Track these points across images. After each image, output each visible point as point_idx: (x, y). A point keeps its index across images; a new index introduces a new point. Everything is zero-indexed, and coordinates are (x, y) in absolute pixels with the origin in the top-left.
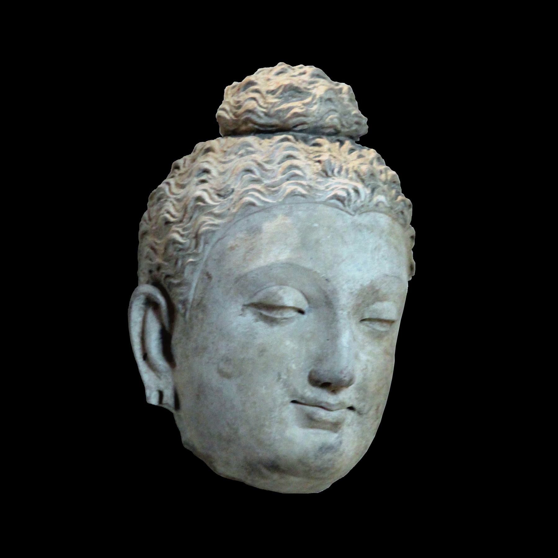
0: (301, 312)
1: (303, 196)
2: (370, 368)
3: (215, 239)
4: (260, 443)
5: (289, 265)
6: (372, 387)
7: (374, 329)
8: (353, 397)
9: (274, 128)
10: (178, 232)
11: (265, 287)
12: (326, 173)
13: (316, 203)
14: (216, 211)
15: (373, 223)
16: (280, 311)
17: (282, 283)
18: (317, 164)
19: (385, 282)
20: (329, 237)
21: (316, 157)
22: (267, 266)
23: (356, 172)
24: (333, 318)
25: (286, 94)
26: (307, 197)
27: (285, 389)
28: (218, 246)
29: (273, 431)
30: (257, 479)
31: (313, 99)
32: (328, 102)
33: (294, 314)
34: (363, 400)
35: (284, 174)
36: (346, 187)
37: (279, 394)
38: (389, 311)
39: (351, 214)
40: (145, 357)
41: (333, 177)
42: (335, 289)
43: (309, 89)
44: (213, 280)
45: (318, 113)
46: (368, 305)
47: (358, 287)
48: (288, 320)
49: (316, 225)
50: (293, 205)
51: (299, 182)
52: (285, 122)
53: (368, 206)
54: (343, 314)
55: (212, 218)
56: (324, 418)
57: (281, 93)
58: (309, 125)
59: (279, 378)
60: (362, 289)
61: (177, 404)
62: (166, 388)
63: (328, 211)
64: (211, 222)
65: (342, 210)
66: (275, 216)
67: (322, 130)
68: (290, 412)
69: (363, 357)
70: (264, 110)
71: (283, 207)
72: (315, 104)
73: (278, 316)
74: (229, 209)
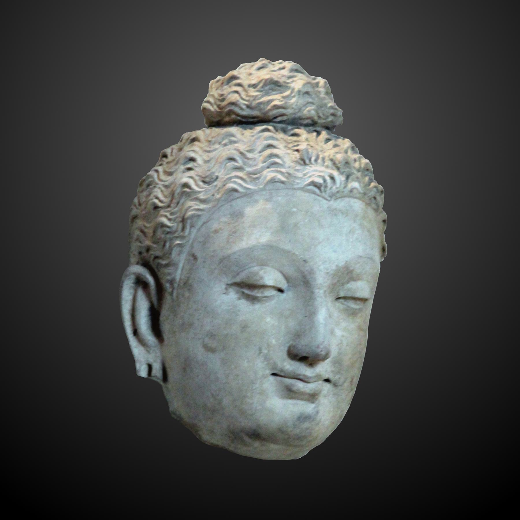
0: (281, 291)
1: (282, 182)
2: (345, 343)
3: (200, 223)
4: (242, 413)
5: (269, 247)
6: (346, 361)
7: (348, 307)
8: (329, 370)
9: (255, 120)
10: (166, 216)
11: (247, 267)
12: (304, 162)
13: (295, 189)
14: (202, 196)
15: (348, 208)
16: (261, 290)
17: (263, 264)
18: (296, 153)
19: (359, 263)
20: (306, 221)
21: (294, 146)
22: (249, 248)
23: (332, 160)
24: (310, 297)
25: (267, 88)
26: (286, 184)
27: (266, 363)
28: (203, 229)
29: (254, 402)
30: (239, 446)
31: (292, 93)
32: (306, 95)
33: (274, 292)
34: (339, 372)
35: (264, 162)
36: (322, 174)
37: (260, 367)
38: (362, 290)
39: (327, 200)
40: (136, 332)
41: (311, 165)
42: (312, 270)
43: (288, 83)
44: (199, 261)
45: (296, 105)
46: (343, 284)
47: (334, 268)
48: (269, 298)
49: (295, 210)
50: (273, 191)
51: (279, 169)
52: (265, 113)
53: (343, 192)
54: (319, 293)
55: (198, 203)
56: (302, 390)
57: (262, 87)
58: (288, 117)
59: (260, 353)
60: (337, 270)
61: (165, 377)
62: (155, 361)
63: (306, 196)
64: (197, 207)
65: (318, 195)
66: (256, 201)
67: (300, 121)
68: (270, 384)
69: (339, 333)
70: (246, 103)
71: (264, 193)
72: (294, 97)
73: (259, 295)
74: (213, 195)
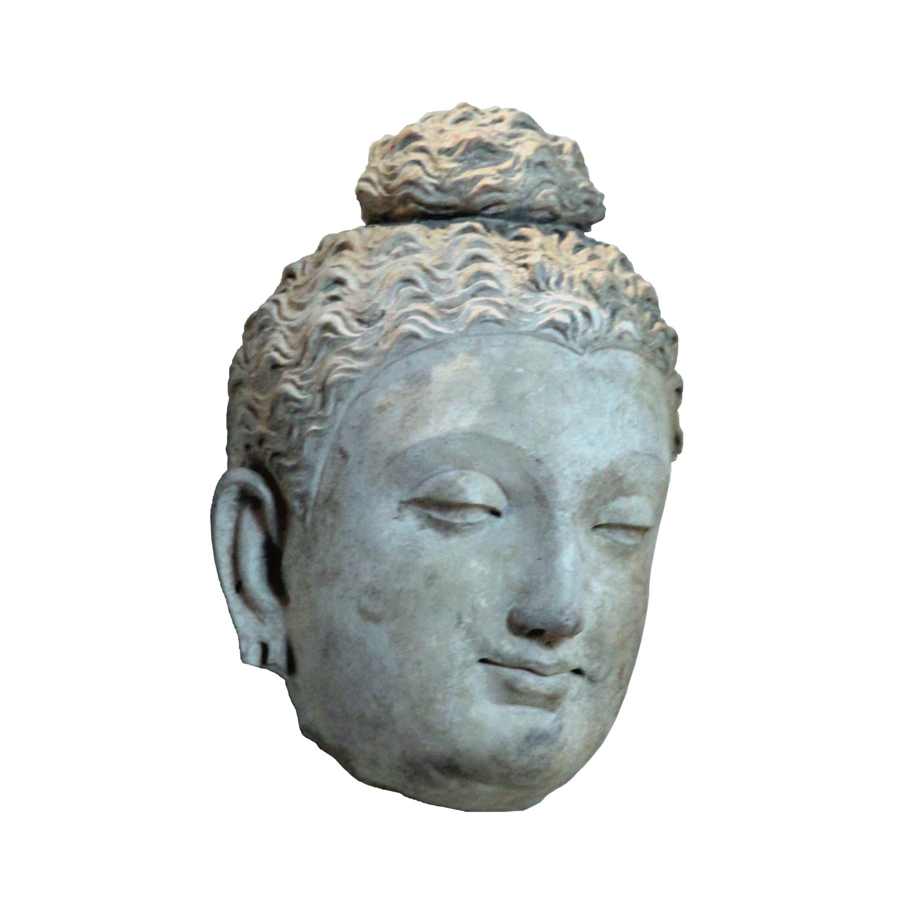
0: (496, 513)
1: (498, 322)
2: (608, 605)
3: (353, 394)
4: (428, 728)
5: (476, 436)
7: (615, 541)
8: (581, 652)
9: (451, 211)
10: (293, 382)
11: (436, 472)
12: (536, 285)
13: (520, 333)
14: (356, 347)
15: (614, 368)
16: (461, 512)
17: (464, 466)
18: (522, 270)
19: (634, 464)
20: (541, 390)
21: (519, 258)
22: (439, 438)
23: (585, 282)
24: (548, 524)
25: (471, 155)
26: (506, 324)
27: (469, 640)
28: (359, 405)
29: (449, 710)
30: (422, 788)
31: (515, 164)
32: (540, 168)
33: (484, 516)
34: (598, 657)
35: (467, 286)
36: (568, 307)
37: (459, 647)
38: (640, 512)
39: (577, 353)
41: (548, 292)
42: (551, 476)
43: (508, 147)
44: (351, 461)
45: (523, 186)
46: (605, 502)
47: (589, 472)
48: (474, 526)
49: (520, 370)
50: (482, 337)
51: (492, 299)
52: (468, 200)
53: (605, 339)
54: (564, 517)
55: (349, 359)
56: (533, 688)
57: (463, 154)
58: (509, 206)
59: (460, 623)
60: (595, 476)
62: (273, 638)
63: (540, 347)
64: (348, 366)
65: (562, 345)
66: (453, 355)
67: (529, 214)
68: (477, 678)
69: (598, 587)
70: (435, 181)
71: (466, 340)
72: (519, 170)
73: (458, 520)
74: (377, 344)
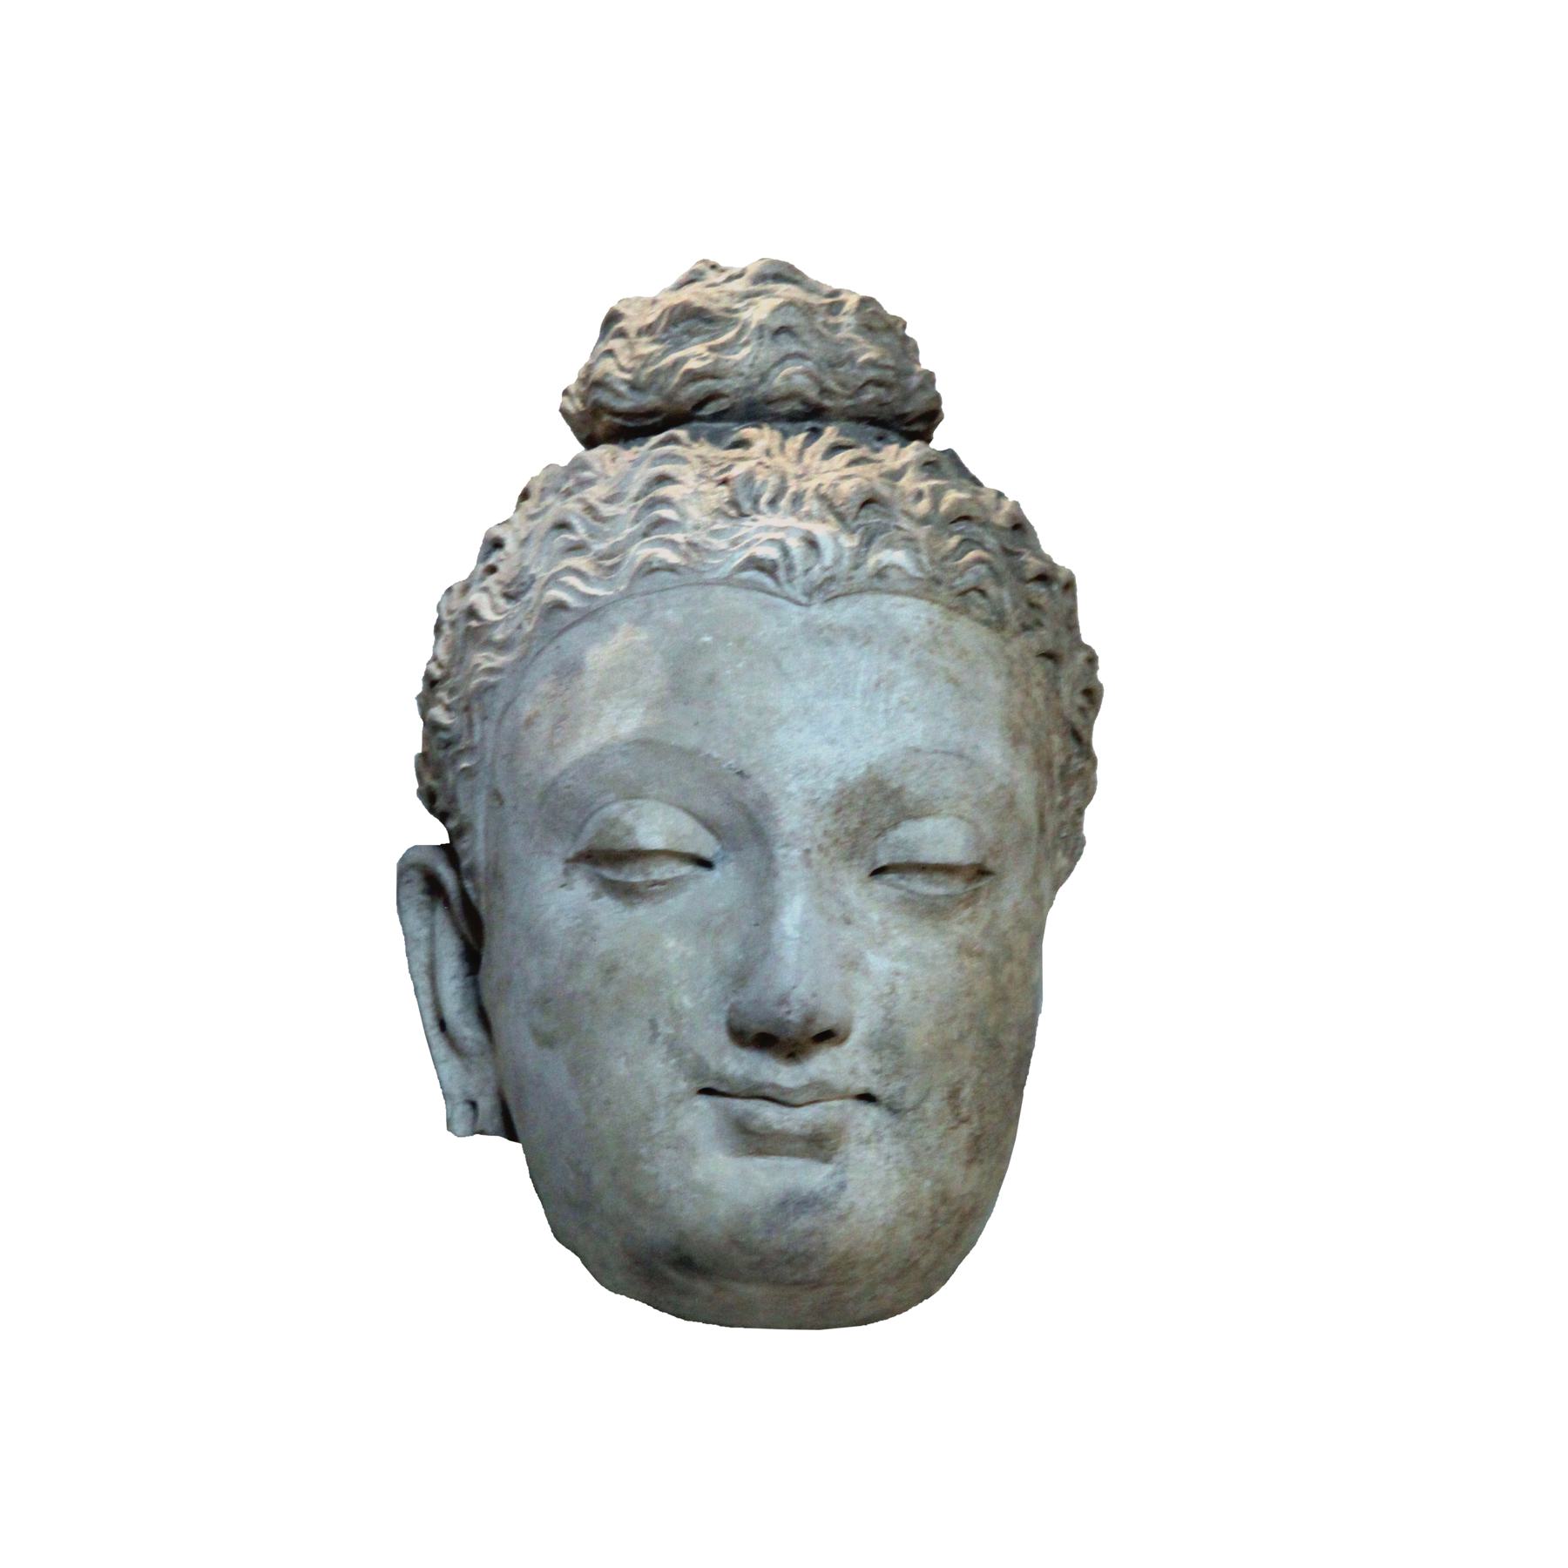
0: (706, 864)
1: (672, 569)
2: (903, 990)
3: (499, 705)
4: (639, 1202)
5: (644, 744)
6: (918, 1038)
7: (912, 892)
8: (863, 1068)
12: (737, 509)
13: (707, 583)
16: (638, 865)
17: (633, 793)
18: (722, 488)
19: (914, 767)
20: (740, 665)
21: (722, 471)
22: (591, 755)
23: (823, 498)
24: (768, 869)
25: (675, 331)
26: (687, 573)
27: (673, 1061)
28: (507, 723)
29: (663, 1169)
31: (740, 334)
33: (686, 869)
34: (897, 1071)
35: (636, 521)
36: (779, 535)
37: (659, 1070)
38: (940, 842)
39: (798, 603)
41: (754, 516)
42: (765, 795)
43: (736, 311)
44: (509, 803)
45: (751, 366)
46: (882, 831)
48: (669, 886)
49: (707, 639)
50: (654, 596)
51: (668, 536)
52: (669, 398)
53: (851, 578)
54: (789, 857)
55: (492, 655)
56: (777, 1127)
57: (665, 330)
58: (733, 399)
59: (655, 1035)
60: (841, 792)
62: (481, 1093)
63: (739, 601)
64: (488, 664)
66: (613, 628)
67: (771, 408)
68: (701, 1117)
69: (879, 963)
70: (627, 376)
71: (631, 603)
72: (746, 344)
73: (637, 879)
74: (520, 627)
